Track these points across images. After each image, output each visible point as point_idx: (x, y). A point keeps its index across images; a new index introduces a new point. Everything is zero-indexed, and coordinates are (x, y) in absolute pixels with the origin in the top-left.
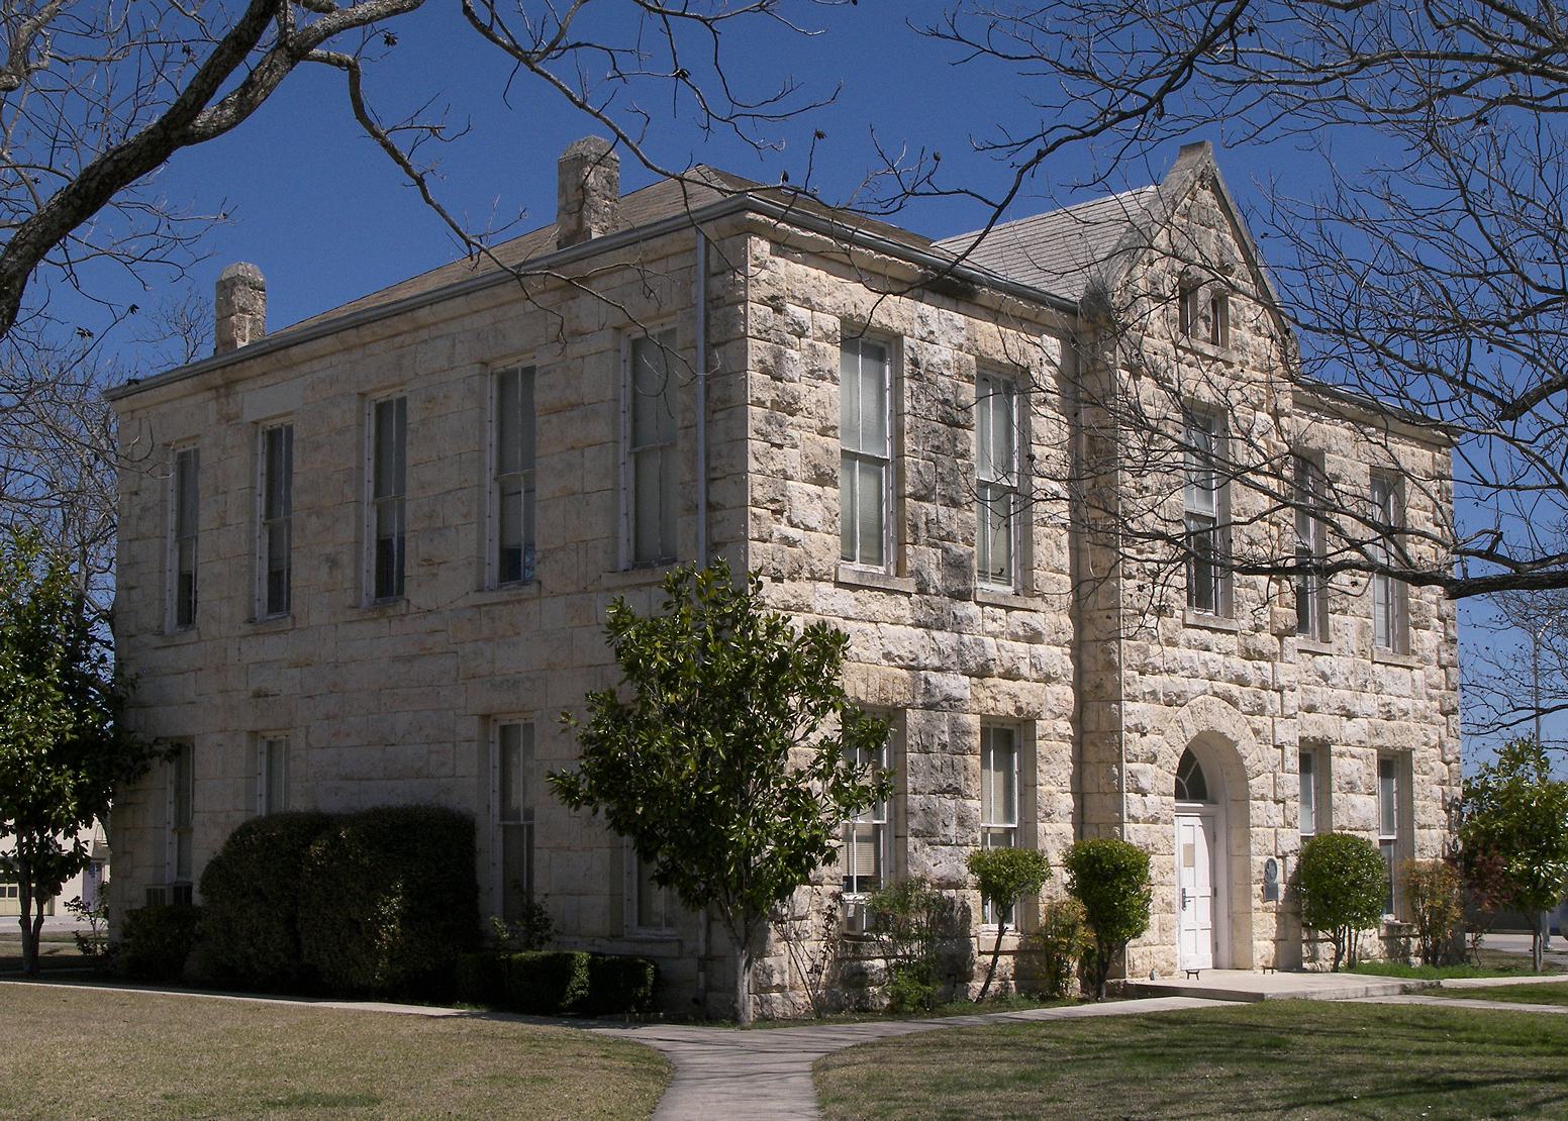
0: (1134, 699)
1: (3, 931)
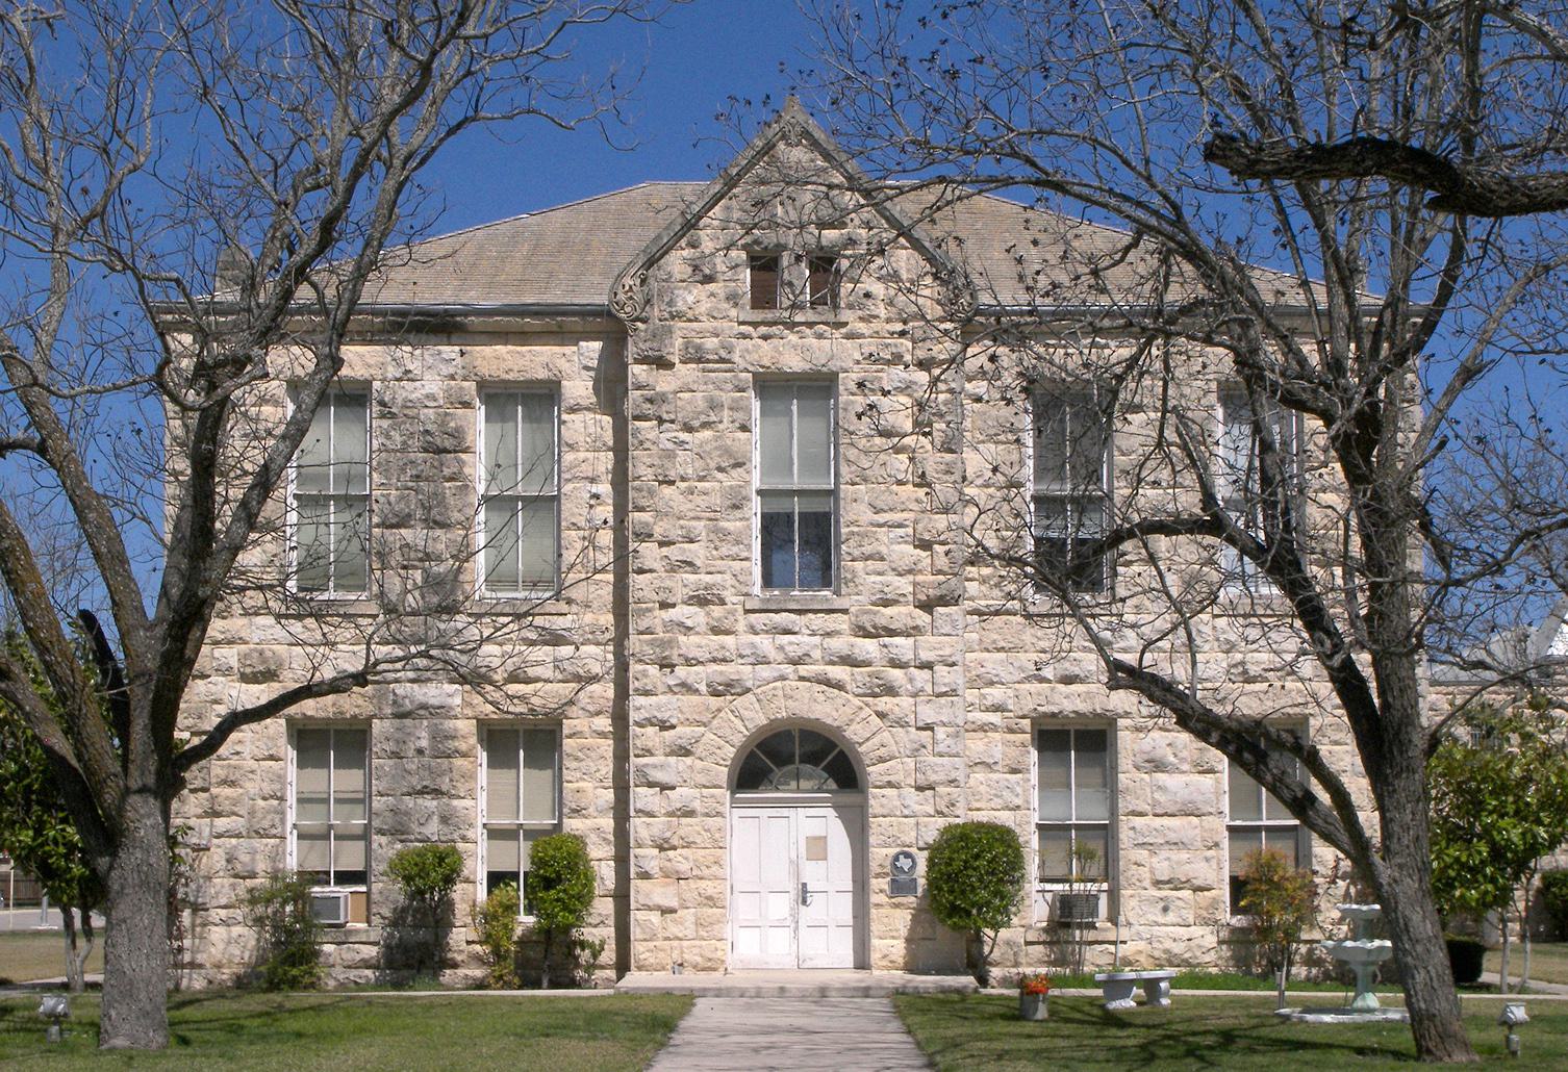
0: (647, 693)
1: (1560, 948)
